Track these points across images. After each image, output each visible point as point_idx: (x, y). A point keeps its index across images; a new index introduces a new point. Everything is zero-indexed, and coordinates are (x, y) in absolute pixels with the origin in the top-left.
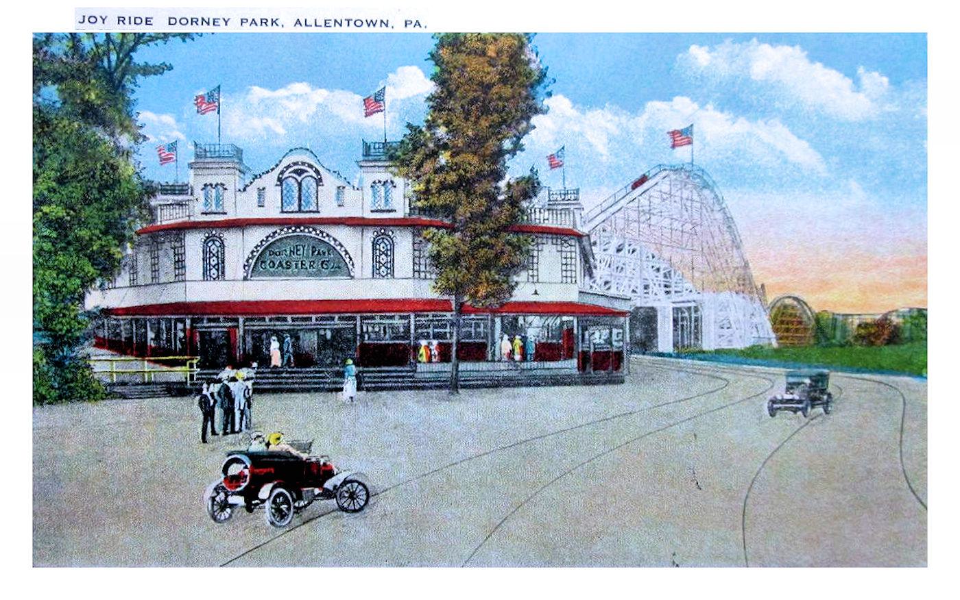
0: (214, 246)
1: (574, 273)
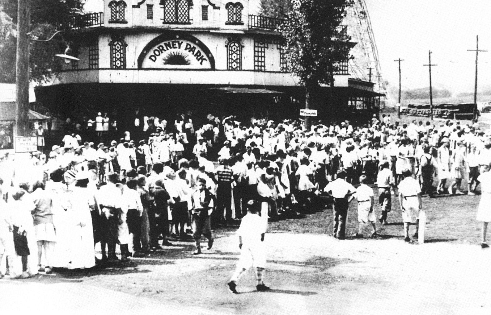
0: (118, 45)
1: (263, 58)
